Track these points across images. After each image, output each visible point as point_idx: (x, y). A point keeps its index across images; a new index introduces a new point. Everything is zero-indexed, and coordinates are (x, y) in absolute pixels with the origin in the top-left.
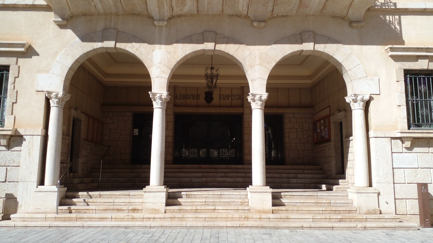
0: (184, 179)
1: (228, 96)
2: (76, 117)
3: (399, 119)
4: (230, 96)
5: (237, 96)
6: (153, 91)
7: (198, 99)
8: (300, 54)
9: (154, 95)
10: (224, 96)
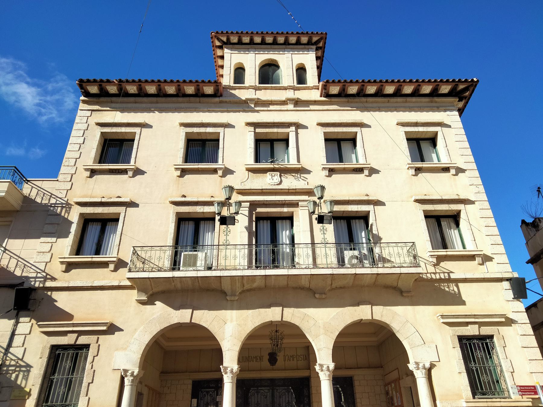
2: (140, 392)
3: (462, 387)
4: (295, 356)
6: (225, 365)
7: (261, 362)
8: (360, 322)
9: (226, 368)
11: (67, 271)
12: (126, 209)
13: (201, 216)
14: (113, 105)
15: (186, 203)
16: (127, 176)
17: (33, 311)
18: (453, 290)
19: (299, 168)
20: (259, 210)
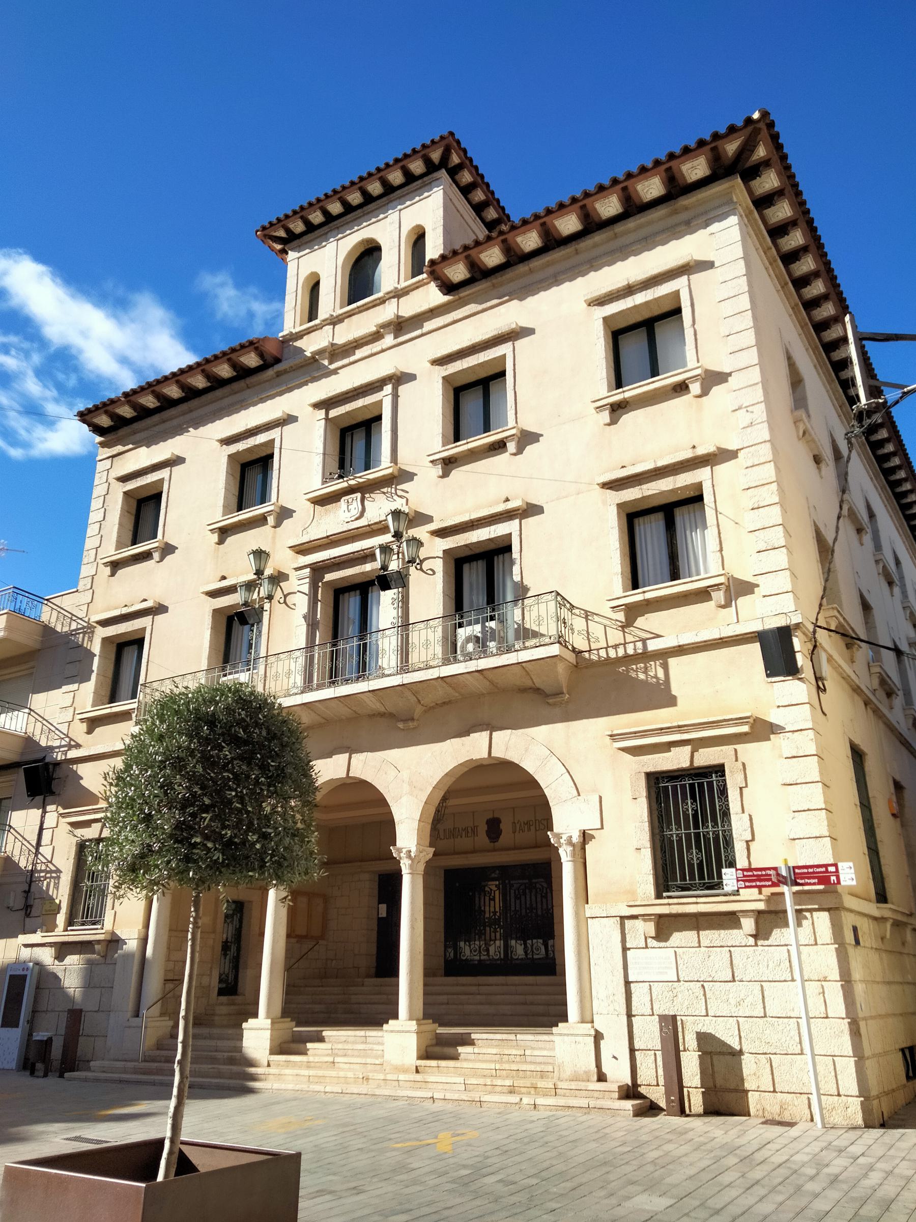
9: (558, 836)
11: (90, 731)
12: (153, 618)
13: (492, 546)
14: (138, 436)
15: (700, 460)
16: (507, 454)
17: (59, 794)
18: (656, 677)
19: (391, 474)
20: (329, 577)
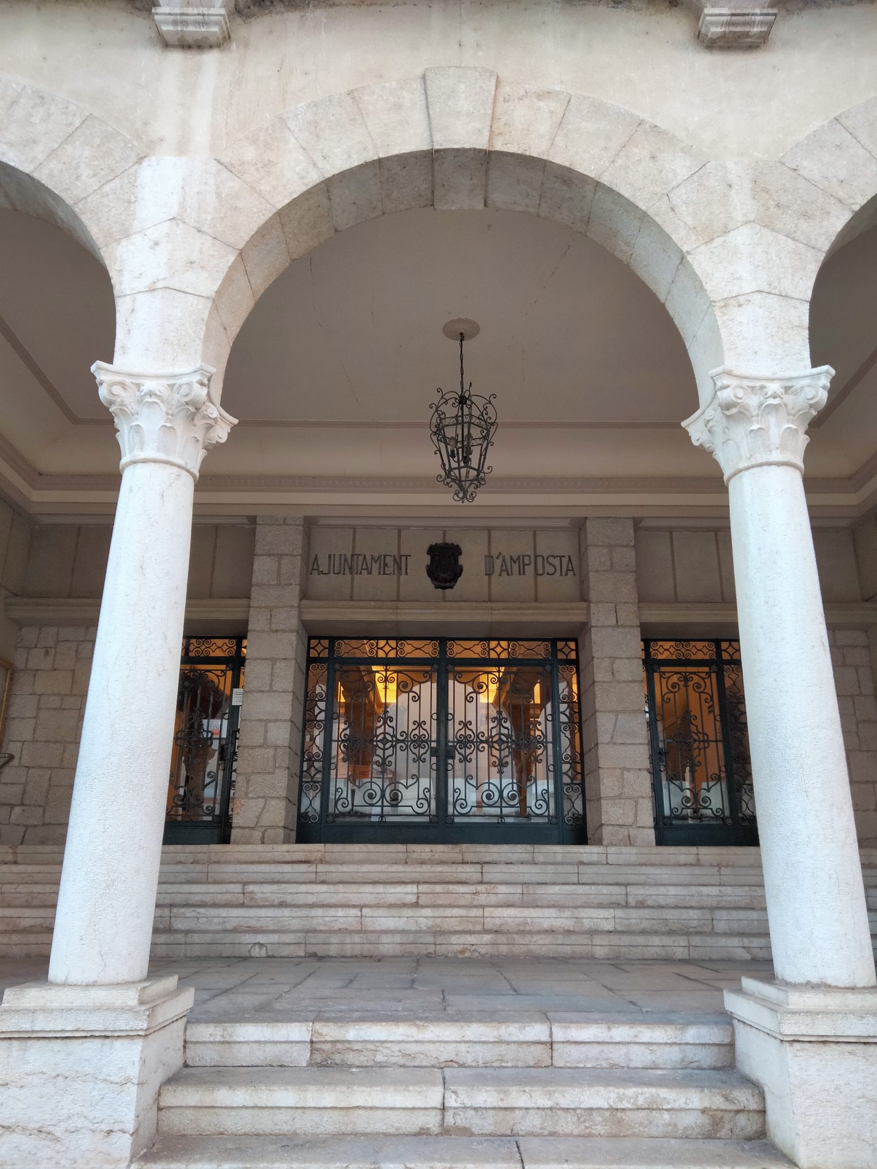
0: (332, 912)
1: (520, 561)
5: (556, 562)
10: (504, 561)
12: (794, 466)
